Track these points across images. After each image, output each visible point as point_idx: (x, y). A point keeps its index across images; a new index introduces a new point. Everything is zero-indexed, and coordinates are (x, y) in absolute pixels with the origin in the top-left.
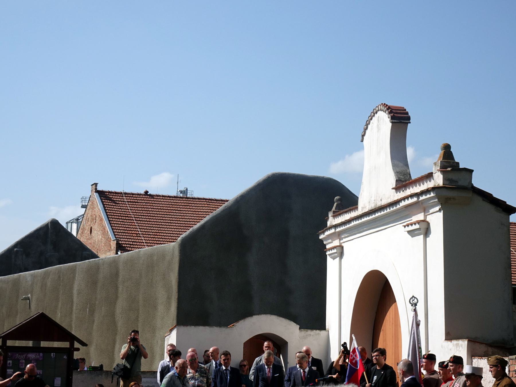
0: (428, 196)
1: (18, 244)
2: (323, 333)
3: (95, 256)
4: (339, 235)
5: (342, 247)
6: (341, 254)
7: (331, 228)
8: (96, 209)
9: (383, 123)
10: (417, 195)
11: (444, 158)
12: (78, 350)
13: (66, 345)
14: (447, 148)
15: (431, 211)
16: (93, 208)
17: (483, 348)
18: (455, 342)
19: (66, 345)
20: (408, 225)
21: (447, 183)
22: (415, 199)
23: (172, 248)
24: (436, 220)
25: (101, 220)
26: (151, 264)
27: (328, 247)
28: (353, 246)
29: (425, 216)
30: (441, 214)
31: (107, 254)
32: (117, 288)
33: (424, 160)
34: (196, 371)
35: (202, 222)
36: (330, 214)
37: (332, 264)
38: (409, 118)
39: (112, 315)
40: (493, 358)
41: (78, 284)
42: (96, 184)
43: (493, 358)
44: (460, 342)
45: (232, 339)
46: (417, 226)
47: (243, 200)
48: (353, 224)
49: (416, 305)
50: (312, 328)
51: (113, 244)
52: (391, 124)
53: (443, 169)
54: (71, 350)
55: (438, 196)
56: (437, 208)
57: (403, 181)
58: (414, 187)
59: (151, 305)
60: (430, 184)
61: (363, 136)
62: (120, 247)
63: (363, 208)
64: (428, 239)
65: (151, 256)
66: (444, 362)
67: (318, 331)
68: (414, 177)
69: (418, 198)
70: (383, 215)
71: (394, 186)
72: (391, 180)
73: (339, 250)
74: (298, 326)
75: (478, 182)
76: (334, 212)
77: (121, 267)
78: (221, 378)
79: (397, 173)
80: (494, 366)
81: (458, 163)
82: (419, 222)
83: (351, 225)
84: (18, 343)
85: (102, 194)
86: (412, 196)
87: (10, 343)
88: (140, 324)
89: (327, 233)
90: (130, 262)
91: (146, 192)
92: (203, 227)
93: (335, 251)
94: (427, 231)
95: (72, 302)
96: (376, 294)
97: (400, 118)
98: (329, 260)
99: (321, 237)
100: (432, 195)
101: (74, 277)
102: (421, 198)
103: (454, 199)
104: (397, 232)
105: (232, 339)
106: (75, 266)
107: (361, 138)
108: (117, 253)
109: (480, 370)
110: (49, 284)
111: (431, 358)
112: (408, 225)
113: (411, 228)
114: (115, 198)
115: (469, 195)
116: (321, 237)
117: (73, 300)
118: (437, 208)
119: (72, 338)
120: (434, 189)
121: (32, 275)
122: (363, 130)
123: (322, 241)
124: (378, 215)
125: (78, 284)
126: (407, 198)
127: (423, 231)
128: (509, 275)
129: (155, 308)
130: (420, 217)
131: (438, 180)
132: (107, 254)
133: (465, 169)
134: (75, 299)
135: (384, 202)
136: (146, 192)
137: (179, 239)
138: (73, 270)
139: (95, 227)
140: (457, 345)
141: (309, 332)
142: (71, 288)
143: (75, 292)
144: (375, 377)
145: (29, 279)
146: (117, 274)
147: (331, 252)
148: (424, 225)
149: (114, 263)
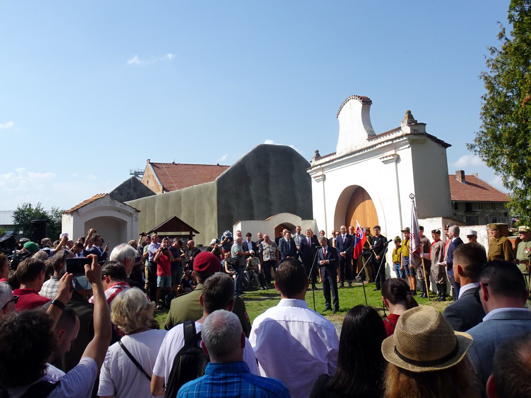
0: (401, 139)
3: (154, 194)
4: (322, 169)
5: (325, 176)
7: (314, 167)
9: (358, 105)
10: (392, 140)
11: (409, 118)
12: (194, 236)
13: (188, 233)
14: (409, 112)
15: (401, 148)
16: (148, 171)
19: (188, 233)
20: (383, 158)
22: (390, 142)
23: (213, 184)
24: (406, 154)
25: (153, 177)
26: (200, 193)
28: (331, 174)
31: (159, 193)
32: (181, 207)
34: (270, 244)
37: (316, 187)
38: (371, 101)
40: (493, 225)
46: (392, 157)
48: (335, 162)
50: (310, 219)
51: (161, 188)
53: (409, 124)
55: (409, 140)
56: (407, 146)
57: (372, 136)
58: (34, 207)
59: (202, 213)
60: (399, 134)
62: (164, 189)
64: (398, 164)
65: (200, 189)
66: (435, 230)
67: (310, 221)
68: (377, 134)
69: (393, 141)
70: (355, 156)
71: (367, 138)
72: (365, 135)
73: (323, 177)
77: (182, 196)
78: (286, 246)
79: (367, 131)
80: (494, 230)
82: (393, 155)
83: (333, 162)
85: (152, 164)
86: (387, 141)
88: (195, 224)
93: (321, 177)
94: (397, 159)
95: (155, 214)
97: (366, 102)
98: (313, 182)
100: (405, 138)
101: (155, 202)
102: (395, 142)
104: (375, 162)
107: (336, 116)
109: (476, 232)
112: (383, 158)
113: (385, 159)
114: (159, 166)
118: (407, 146)
119: (191, 230)
122: (338, 111)
123: (308, 173)
124: (356, 155)
127: (395, 160)
129: (204, 215)
130: (393, 152)
131: (407, 130)
132: (159, 193)
133: (422, 124)
134: (156, 213)
135: (359, 148)
137: (217, 179)
139: (151, 181)
142: (154, 209)
143: (156, 210)
144: (375, 242)
146: (180, 199)
148: (396, 157)
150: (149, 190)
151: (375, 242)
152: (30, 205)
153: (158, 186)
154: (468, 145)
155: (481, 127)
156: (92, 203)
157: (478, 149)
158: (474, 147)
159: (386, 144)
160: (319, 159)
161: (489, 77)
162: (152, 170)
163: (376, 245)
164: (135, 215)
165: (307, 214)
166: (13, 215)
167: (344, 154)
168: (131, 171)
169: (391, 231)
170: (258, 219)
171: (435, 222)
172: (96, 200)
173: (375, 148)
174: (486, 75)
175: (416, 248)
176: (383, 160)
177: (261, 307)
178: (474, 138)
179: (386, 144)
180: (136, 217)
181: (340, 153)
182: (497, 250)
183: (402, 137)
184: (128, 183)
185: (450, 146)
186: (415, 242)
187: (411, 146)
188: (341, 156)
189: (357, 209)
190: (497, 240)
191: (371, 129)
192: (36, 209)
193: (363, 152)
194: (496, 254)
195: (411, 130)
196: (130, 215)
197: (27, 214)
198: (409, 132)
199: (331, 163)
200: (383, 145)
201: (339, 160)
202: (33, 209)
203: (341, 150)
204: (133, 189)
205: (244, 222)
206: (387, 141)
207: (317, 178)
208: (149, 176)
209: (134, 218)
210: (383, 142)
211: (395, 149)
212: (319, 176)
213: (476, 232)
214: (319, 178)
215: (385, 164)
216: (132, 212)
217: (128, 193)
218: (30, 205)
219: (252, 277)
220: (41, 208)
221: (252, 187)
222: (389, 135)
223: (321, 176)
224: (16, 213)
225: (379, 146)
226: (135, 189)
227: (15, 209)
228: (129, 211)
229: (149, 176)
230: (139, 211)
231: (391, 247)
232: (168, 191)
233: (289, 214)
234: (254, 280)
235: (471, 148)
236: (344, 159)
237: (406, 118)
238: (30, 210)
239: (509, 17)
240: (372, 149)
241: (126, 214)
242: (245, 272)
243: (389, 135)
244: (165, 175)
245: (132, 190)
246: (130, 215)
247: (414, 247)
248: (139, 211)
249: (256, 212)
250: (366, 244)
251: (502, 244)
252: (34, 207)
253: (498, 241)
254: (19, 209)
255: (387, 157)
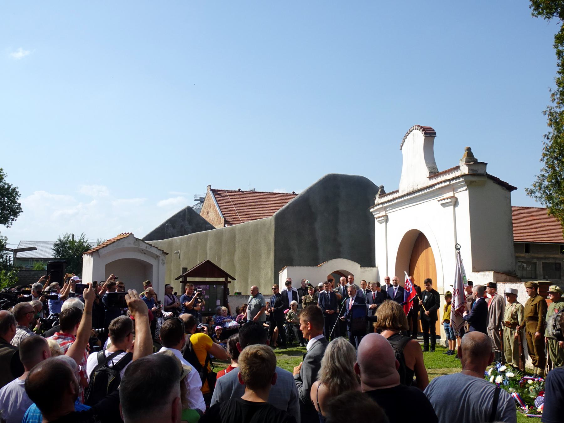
0: (458, 181)
1: (167, 222)
2: (374, 268)
3: (213, 228)
4: (385, 209)
5: (387, 216)
6: (387, 220)
7: (379, 204)
8: (211, 200)
9: (419, 137)
10: (449, 180)
12: (230, 282)
13: (222, 279)
14: (469, 150)
16: (209, 200)
17: (503, 277)
18: (482, 273)
19: (222, 279)
20: (441, 200)
21: (471, 172)
22: (448, 183)
23: (270, 220)
24: (463, 196)
25: (214, 206)
26: (256, 230)
27: (375, 216)
28: (393, 215)
29: (454, 194)
30: (467, 192)
31: (219, 226)
32: (235, 246)
33: (452, 158)
35: (288, 204)
36: (377, 196)
37: (379, 228)
38: (435, 133)
39: (233, 260)
40: (529, 283)
41: (210, 244)
42: (210, 186)
43: (529, 283)
44: (487, 273)
45: (318, 276)
46: (449, 200)
47: (311, 191)
48: (396, 201)
49: (459, 249)
52: (424, 137)
53: (468, 163)
54: (225, 284)
55: (465, 181)
56: (464, 188)
57: (434, 173)
58: (77, 239)
61: (402, 146)
62: (226, 222)
63: (403, 191)
64: (456, 208)
65: (256, 225)
67: (371, 268)
68: (440, 171)
69: (450, 182)
70: (417, 195)
71: (428, 176)
72: (426, 172)
73: (386, 218)
74: (360, 265)
75: (490, 171)
76: (380, 195)
77: (237, 232)
78: (325, 298)
79: (429, 168)
81: (477, 159)
82: (450, 198)
83: (395, 202)
84: (197, 279)
85: (214, 191)
86: (445, 181)
87: (189, 279)
89: (376, 208)
90: (233, 231)
91: (239, 190)
92: (288, 207)
93: (383, 218)
94: (455, 202)
96: (415, 245)
97: (430, 134)
98: (377, 224)
99: (371, 210)
100: (461, 179)
101: (207, 239)
102: (452, 182)
103: (475, 182)
104: (433, 204)
105: (318, 276)
106: (208, 233)
107: (400, 148)
108: (225, 226)
109: (516, 291)
110: (191, 244)
111: (470, 283)
112: (441, 200)
113: (443, 202)
115: (486, 179)
116: (371, 210)
117: (207, 253)
118: (464, 188)
120: (463, 176)
121: (180, 239)
123: (371, 213)
124: (416, 194)
125: (210, 244)
126: (438, 183)
127: (453, 203)
128: (511, 232)
130: (451, 194)
131: (465, 170)
132: (219, 226)
134: (208, 252)
135: (420, 187)
136: (239, 190)
137: (275, 214)
138: (206, 235)
139: (211, 211)
140: (484, 275)
141: (367, 269)
142: (206, 246)
143: (208, 248)
144: (426, 297)
145: (178, 241)
146: (235, 237)
147: (378, 220)
148: (454, 200)
149: (221, 232)
150: (205, 222)
151: (426, 297)
152: (73, 236)
153: (219, 218)
154: (527, 190)
155: (542, 170)
156: (115, 244)
157: (539, 195)
158: (535, 192)
159: (444, 184)
160: (383, 197)
161: (556, 112)
162: (213, 198)
163: (427, 300)
164: (162, 257)
165: (368, 260)
166: (53, 248)
167: (406, 192)
168: (195, 196)
169: (445, 283)
170: (299, 265)
171: (488, 277)
172: (118, 240)
173: (433, 188)
174: (552, 111)
175: (459, 305)
176: (441, 202)
177: (286, 365)
178: (533, 182)
179: (444, 184)
180: (163, 260)
181: (403, 191)
182: (530, 311)
183: (458, 177)
184: (182, 214)
185: (516, 188)
186: (459, 299)
187: (469, 188)
188: (403, 194)
189: (420, 257)
190: (532, 299)
191: (433, 165)
192: (80, 241)
193: (423, 192)
194: (529, 315)
195: (469, 170)
196: (157, 257)
197: (68, 247)
198: (467, 172)
199: (393, 203)
200: (441, 185)
201: (400, 200)
202: (76, 242)
203: (404, 188)
204: (187, 222)
205: (291, 268)
206: (445, 181)
207: (379, 219)
208: (209, 206)
209: (161, 261)
210: (441, 182)
211: (454, 191)
212: (382, 217)
213: (516, 291)
214: (381, 219)
215: (444, 207)
216: (158, 255)
217: (182, 226)
218: (73, 236)
219: (291, 331)
220: (85, 240)
221: (318, 225)
222: (449, 174)
223: (383, 216)
224: (56, 245)
225: (438, 186)
226: (190, 222)
227: (56, 240)
228: (155, 253)
229: (209, 206)
230: (167, 254)
231: (443, 302)
232: (231, 224)
233: (339, 260)
234: (293, 336)
235: (531, 194)
236: (405, 198)
237: (464, 156)
238: (72, 242)
239: (557, 53)
240: (431, 190)
241: (152, 257)
242: (284, 325)
243: (449, 174)
244: (229, 204)
245: (187, 222)
246: (157, 257)
247: (456, 304)
248: (167, 254)
249: (321, 253)
250: (416, 301)
251: (536, 304)
252: (77, 239)
253: (533, 301)
254: (60, 240)
255: (444, 199)
